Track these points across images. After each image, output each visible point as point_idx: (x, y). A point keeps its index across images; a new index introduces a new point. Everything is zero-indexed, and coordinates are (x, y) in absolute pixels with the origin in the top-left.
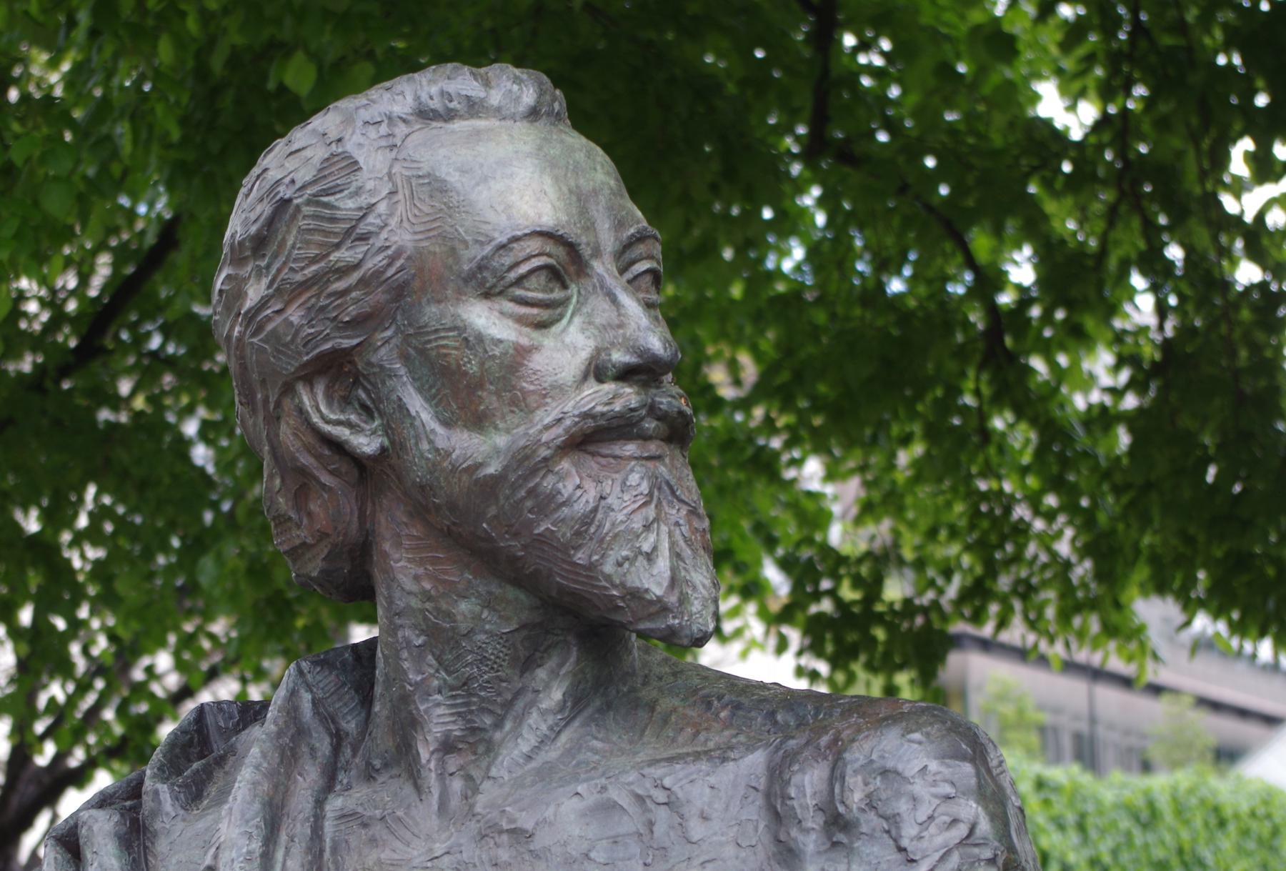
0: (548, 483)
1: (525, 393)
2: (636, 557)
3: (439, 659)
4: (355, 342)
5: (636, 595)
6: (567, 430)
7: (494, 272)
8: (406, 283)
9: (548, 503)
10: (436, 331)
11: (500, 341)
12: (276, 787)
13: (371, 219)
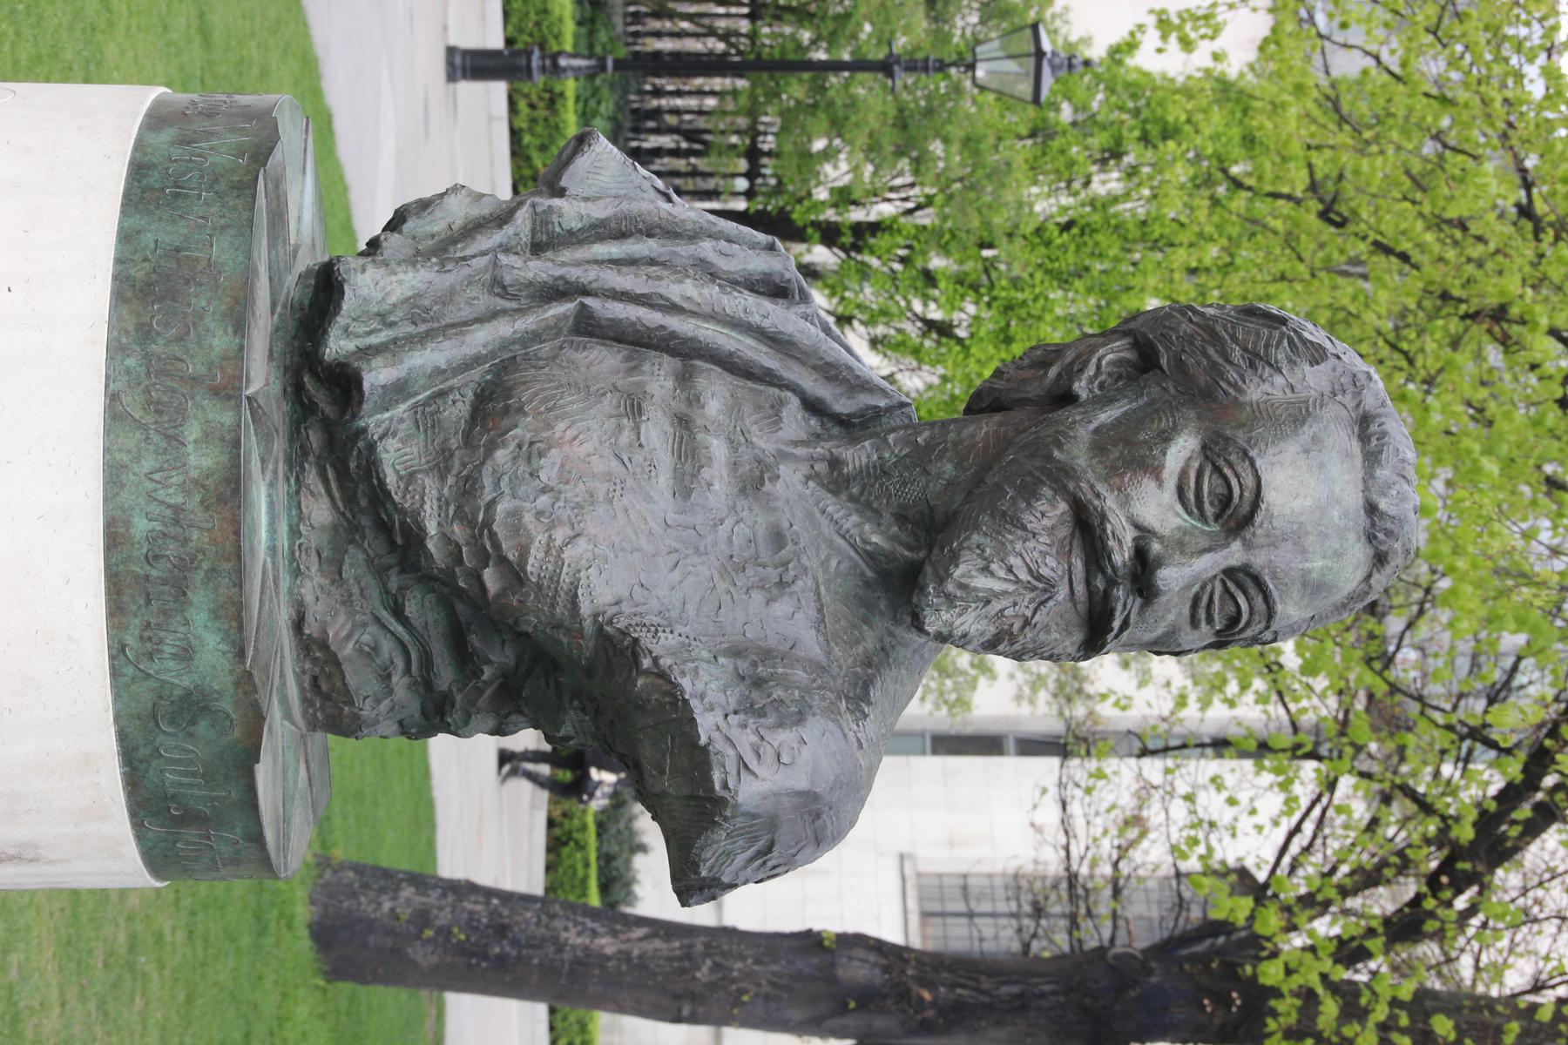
0: (1046, 491)
1: (1122, 475)
2: (985, 559)
3: (906, 455)
4: (1165, 367)
5: (954, 559)
6: (1089, 501)
7: (1225, 449)
8: (1215, 399)
9: (1029, 493)
11: (1165, 454)
12: (805, 353)
13: (1267, 369)
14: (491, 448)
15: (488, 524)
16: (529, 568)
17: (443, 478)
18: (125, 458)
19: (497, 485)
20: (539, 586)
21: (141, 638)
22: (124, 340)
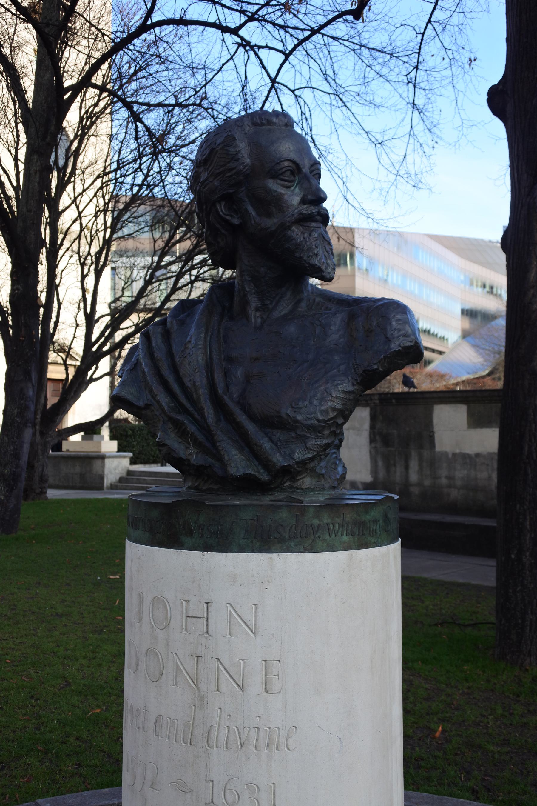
0: (289, 232)
4: (234, 191)
14: (297, 421)
15: (325, 421)
16: (339, 408)
17: (308, 438)
18: (325, 544)
19: (311, 419)
20: (343, 404)
21: (372, 536)
22: (285, 547)
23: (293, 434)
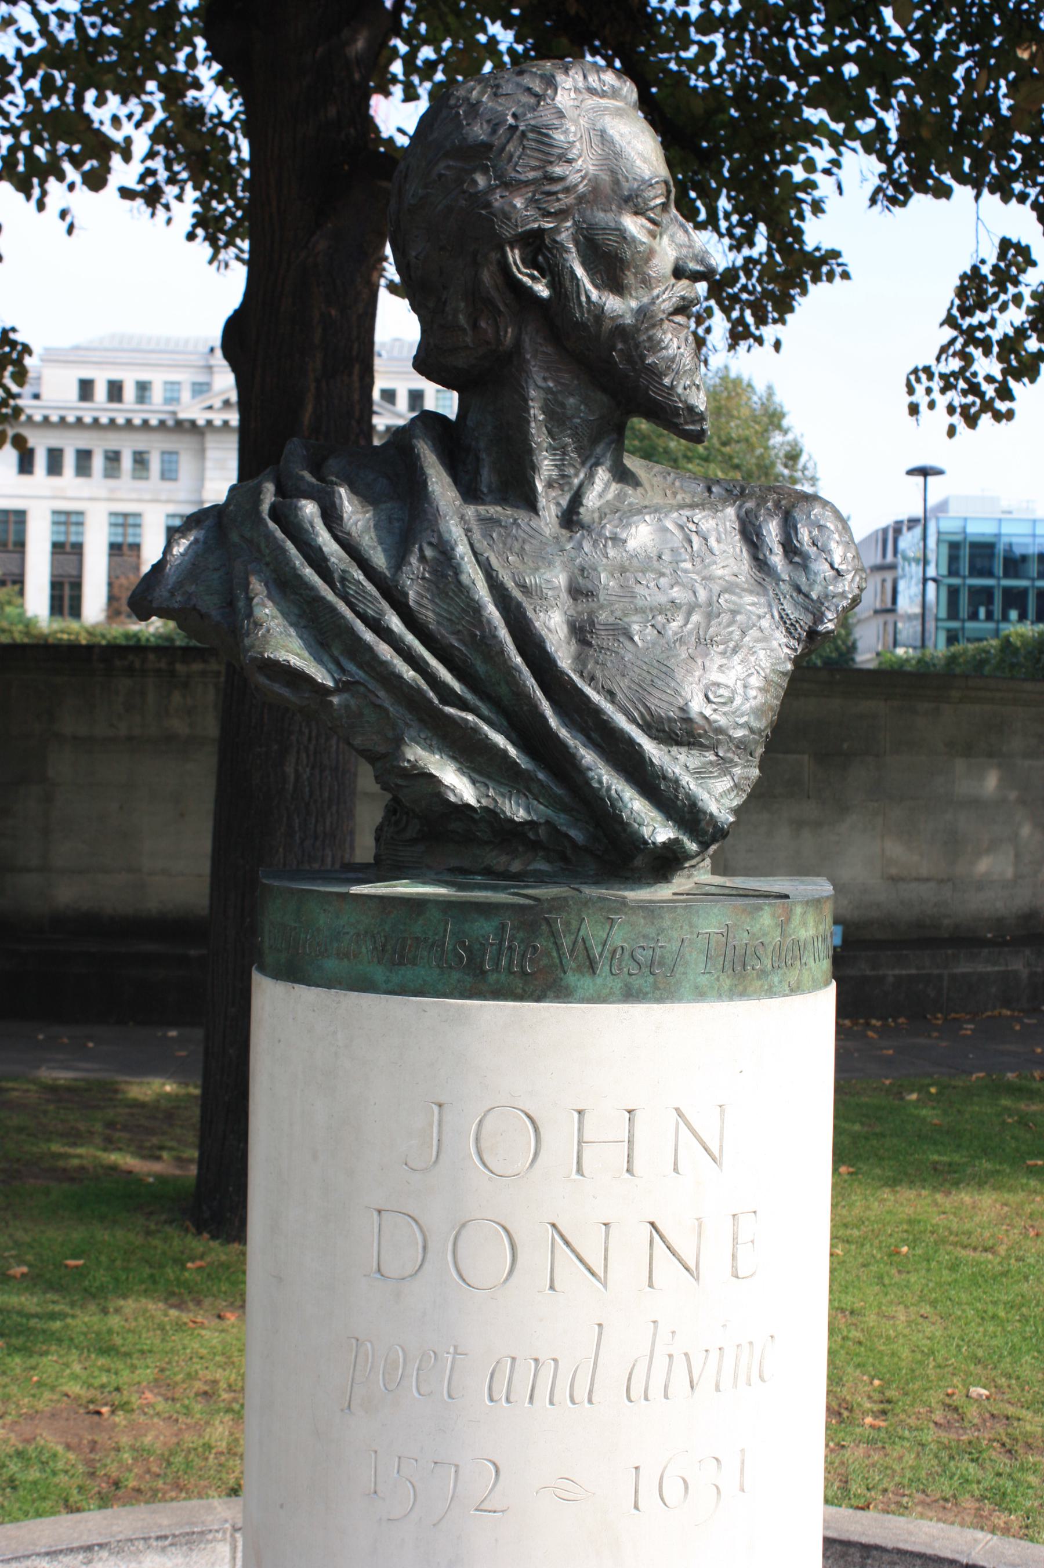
4: (551, 225)
5: (691, 409)
9: (656, 346)
10: (604, 229)
23: (711, 757)
